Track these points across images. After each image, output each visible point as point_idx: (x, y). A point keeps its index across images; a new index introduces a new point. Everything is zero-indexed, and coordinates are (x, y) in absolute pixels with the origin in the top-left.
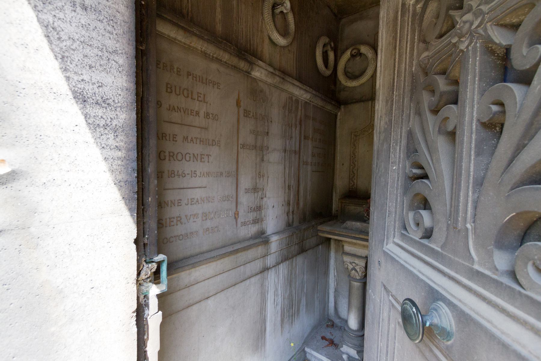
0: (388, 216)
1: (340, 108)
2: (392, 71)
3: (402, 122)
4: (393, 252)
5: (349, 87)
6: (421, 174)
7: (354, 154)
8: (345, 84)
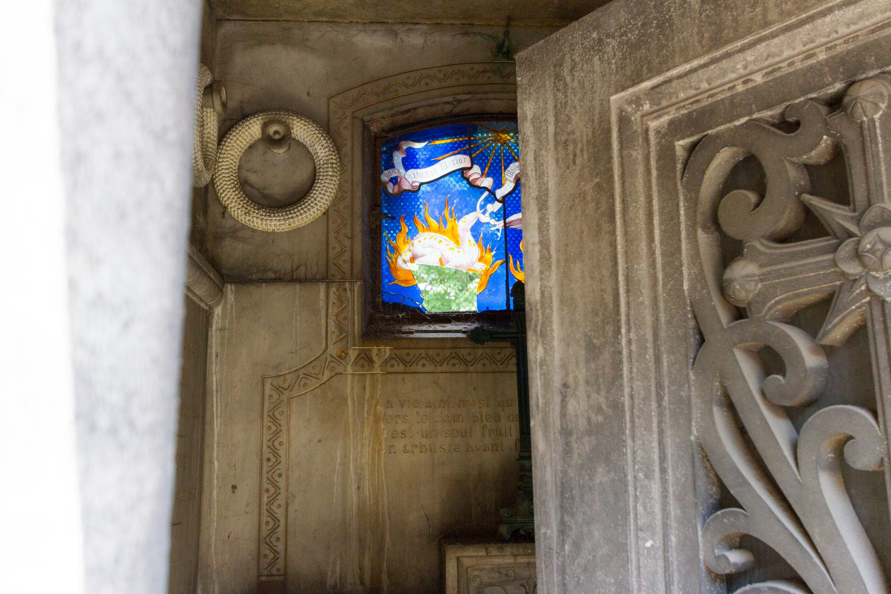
1: (221, 291)
2: (606, 273)
3: (661, 415)
5: (254, 231)
6: (744, 564)
7: (274, 451)
8: (244, 219)
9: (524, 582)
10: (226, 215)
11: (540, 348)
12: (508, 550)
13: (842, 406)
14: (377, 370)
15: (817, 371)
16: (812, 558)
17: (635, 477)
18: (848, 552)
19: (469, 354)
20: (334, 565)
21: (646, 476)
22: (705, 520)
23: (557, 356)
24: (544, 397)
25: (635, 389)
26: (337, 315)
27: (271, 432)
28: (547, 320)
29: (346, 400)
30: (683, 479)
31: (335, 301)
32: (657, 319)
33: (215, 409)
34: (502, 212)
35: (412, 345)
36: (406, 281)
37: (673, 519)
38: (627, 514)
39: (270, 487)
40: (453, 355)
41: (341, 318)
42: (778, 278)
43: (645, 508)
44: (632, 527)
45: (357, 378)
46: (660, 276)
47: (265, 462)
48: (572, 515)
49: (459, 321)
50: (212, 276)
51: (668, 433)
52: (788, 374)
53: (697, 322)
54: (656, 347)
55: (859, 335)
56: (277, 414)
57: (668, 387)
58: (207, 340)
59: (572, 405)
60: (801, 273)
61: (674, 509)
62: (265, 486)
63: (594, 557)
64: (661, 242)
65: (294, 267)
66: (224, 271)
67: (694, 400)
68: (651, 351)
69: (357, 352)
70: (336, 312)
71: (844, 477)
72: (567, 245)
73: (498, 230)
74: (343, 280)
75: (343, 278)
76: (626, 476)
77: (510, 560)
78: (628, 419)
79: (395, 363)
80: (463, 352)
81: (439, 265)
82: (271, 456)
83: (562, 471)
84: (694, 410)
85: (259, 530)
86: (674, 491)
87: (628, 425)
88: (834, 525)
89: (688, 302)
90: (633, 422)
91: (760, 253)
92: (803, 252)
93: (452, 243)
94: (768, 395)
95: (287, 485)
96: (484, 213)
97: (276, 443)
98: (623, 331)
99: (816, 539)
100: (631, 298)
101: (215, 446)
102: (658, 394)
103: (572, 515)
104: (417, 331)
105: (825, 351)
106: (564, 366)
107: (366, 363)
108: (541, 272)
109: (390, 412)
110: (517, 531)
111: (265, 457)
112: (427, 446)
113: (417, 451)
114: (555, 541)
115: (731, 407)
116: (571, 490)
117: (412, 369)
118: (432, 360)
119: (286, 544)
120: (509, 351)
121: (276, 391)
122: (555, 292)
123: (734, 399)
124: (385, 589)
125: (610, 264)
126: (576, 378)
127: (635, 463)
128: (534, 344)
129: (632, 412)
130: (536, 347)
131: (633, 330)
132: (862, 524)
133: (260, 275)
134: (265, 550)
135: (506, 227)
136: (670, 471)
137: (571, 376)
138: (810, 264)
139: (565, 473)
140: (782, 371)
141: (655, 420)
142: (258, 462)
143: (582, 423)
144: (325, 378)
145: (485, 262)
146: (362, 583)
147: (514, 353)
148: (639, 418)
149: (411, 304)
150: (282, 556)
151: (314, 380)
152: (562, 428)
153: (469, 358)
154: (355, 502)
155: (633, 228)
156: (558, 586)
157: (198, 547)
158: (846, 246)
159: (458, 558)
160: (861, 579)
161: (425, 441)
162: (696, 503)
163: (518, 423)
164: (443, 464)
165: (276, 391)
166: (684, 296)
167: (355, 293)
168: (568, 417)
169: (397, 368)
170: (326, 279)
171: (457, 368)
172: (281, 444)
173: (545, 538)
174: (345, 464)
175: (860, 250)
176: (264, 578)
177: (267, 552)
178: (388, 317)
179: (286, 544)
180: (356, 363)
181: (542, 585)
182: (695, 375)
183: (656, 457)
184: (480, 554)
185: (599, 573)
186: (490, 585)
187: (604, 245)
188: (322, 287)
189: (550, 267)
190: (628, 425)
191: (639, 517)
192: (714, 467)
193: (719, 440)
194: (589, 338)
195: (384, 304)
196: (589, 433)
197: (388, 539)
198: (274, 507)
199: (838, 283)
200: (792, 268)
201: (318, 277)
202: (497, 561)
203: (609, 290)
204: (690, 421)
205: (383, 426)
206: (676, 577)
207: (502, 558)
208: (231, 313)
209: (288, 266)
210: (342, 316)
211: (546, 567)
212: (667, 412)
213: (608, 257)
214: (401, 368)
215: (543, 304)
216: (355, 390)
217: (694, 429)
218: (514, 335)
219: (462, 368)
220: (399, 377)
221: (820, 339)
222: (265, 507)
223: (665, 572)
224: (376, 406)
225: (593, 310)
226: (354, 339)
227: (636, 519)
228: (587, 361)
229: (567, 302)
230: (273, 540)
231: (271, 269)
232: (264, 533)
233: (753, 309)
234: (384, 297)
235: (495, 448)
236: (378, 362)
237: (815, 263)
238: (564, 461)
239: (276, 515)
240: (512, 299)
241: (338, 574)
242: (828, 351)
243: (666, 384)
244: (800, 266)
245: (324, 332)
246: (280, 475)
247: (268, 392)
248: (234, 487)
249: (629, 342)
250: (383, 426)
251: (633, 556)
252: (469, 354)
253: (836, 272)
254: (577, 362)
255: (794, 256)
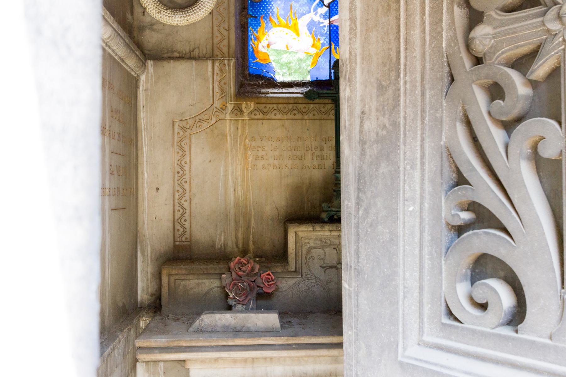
0: (405, 297)
1: (144, 65)
2: (392, 37)
3: (423, 129)
4: (426, 362)
5: (164, 25)
6: (469, 220)
8: (157, 16)
9: (336, 247)
10: (146, 13)
11: (348, 90)
12: (327, 227)
13: (539, 118)
14: (246, 117)
15: (526, 97)
16: (511, 213)
17: (405, 168)
18: (534, 208)
19: (305, 108)
20: (220, 236)
21: (412, 167)
22: (447, 193)
23: (359, 94)
24: (349, 121)
25: (407, 113)
26: (220, 82)
27: (179, 155)
28: (353, 70)
29: (226, 136)
30: (435, 169)
31: (218, 72)
32: (424, 67)
33: (143, 140)
34: (328, 14)
35: (268, 102)
36: (264, 60)
37: (427, 193)
38: (398, 191)
39: (179, 189)
40: (295, 108)
41: (223, 82)
42: (505, 35)
43: (410, 187)
44: (401, 199)
45: (233, 122)
46: (428, 38)
47: (176, 174)
48: (365, 193)
49: (298, 86)
50: (138, 53)
51: (427, 140)
52: (506, 99)
53: (450, 69)
54: (423, 86)
55: (555, 73)
56: (183, 144)
57: (429, 111)
58: (137, 97)
59: (367, 125)
60: (520, 31)
61: (428, 187)
62: (177, 188)
63: (377, 217)
64: (430, 15)
65: (191, 49)
66: (146, 52)
67: (445, 118)
68: (419, 89)
69: (233, 106)
70: (219, 79)
71: (536, 165)
72: (368, 20)
73: (324, 26)
74: (223, 58)
75: (223, 57)
76: (399, 168)
77: (327, 234)
78: (402, 132)
79: (257, 113)
80: (301, 106)
81: (285, 49)
82: (180, 170)
83: (359, 167)
84: (444, 125)
85: (174, 215)
86: (428, 176)
87: (402, 136)
88: (527, 192)
89: (445, 55)
90: (405, 134)
91: (495, 19)
92: (523, 17)
93: (294, 35)
94: (492, 114)
95: (190, 188)
96: (316, 14)
97: (183, 163)
98: (402, 75)
99: (515, 202)
100: (408, 54)
101: (145, 163)
102: (422, 116)
103: (365, 193)
104: (271, 93)
105: (531, 83)
106: (363, 100)
107: (238, 113)
108: (350, 39)
109: (254, 144)
110: (333, 216)
111: (176, 171)
112: (278, 166)
113: (271, 168)
114: (353, 209)
115: (468, 123)
116: (365, 177)
117: (268, 117)
118: (280, 111)
119: (191, 223)
120: (331, 106)
121: (182, 129)
122: (359, 51)
123: (471, 117)
124: (251, 250)
125: (395, 31)
126: (370, 107)
127: (405, 160)
128: (344, 87)
129: (405, 128)
130: (345, 89)
131: (408, 75)
132: (546, 194)
133: (169, 55)
134: (178, 227)
135: (330, 25)
136: (427, 164)
137: (367, 106)
138: (527, 25)
139: (360, 167)
140: (502, 98)
141: (419, 132)
142: (172, 174)
143: (373, 136)
144: (213, 122)
145: (316, 48)
146: (237, 246)
147: (334, 108)
148: (409, 131)
149: (268, 75)
150: (188, 230)
151: (206, 123)
152: (360, 140)
153: (304, 110)
154: (232, 199)
155: (412, 7)
156: (354, 236)
157: (137, 224)
158: (552, 11)
159: (295, 232)
160: (541, 224)
161: (276, 162)
162: (442, 183)
163: (335, 152)
164: (287, 176)
165: (182, 129)
166: (442, 51)
167: (231, 67)
168: (364, 133)
169: (258, 116)
170: (212, 57)
171: (297, 117)
172: (186, 163)
173: (347, 208)
174: (226, 176)
175: (560, 13)
176: (177, 243)
177: (179, 228)
178: (252, 83)
179: (191, 223)
180: (232, 112)
181: (345, 235)
182: (446, 102)
183: (418, 155)
184: (309, 229)
185: (380, 227)
186: (315, 248)
187: (392, 18)
188: (210, 63)
189: (356, 35)
190: (402, 136)
191: (406, 192)
192: (455, 160)
193: (459, 142)
194: (380, 81)
195: (250, 74)
196: (377, 142)
197: (253, 220)
198: (182, 201)
199: (545, 37)
200: (514, 28)
201: (206, 56)
202: (321, 234)
203: (394, 48)
204: (441, 132)
205: (249, 152)
206: (427, 228)
207: (322, 232)
208: (151, 79)
209: (188, 50)
210: (223, 82)
211: (348, 224)
212: (427, 127)
213: (394, 26)
214: (261, 116)
215: (350, 60)
216: (232, 130)
217: (444, 137)
218: (333, 95)
219: (300, 116)
220: (260, 121)
221: (529, 76)
222: (177, 201)
223: (420, 225)
224: (245, 141)
225: (382, 62)
226: (231, 97)
227: (404, 193)
228: (378, 96)
229: (366, 58)
230: (182, 221)
231: (176, 51)
232: (177, 217)
233: (487, 57)
234: (250, 71)
235: (320, 167)
236: (246, 112)
237: (530, 24)
238: (361, 160)
239: (184, 206)
240: (333, 71)
241: (222, 241)
242: (534, 84)
243: (428, 109)
244: (520, 26)
245: (211, 92)
246: (186, 182)
247: (176, 130)
248: (158, 189)
249: (405, 83)
250: (249, 152)
251: (401, 216)
252: (305, 108)
253: (544, 29)
254: (371, 97)
255: (517, 20)
